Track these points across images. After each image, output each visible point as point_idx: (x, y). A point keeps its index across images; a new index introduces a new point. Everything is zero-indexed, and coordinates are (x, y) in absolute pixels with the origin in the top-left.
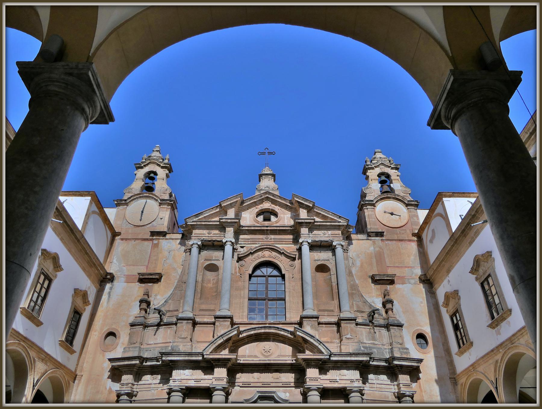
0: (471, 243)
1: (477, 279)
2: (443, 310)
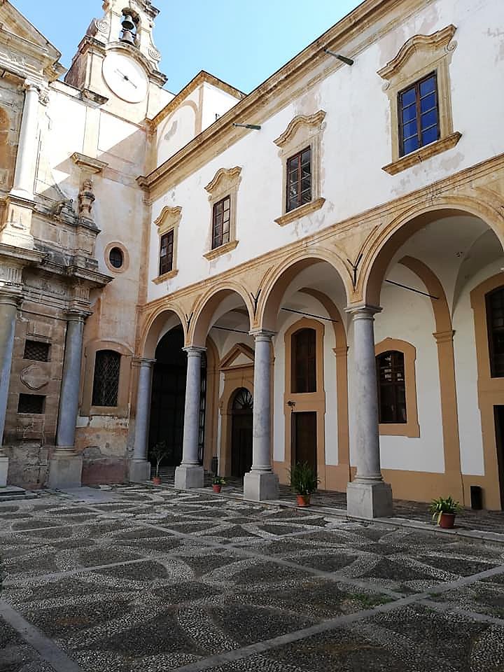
0: (219, 153)
1: (210, 199)
2: (154, 228)
